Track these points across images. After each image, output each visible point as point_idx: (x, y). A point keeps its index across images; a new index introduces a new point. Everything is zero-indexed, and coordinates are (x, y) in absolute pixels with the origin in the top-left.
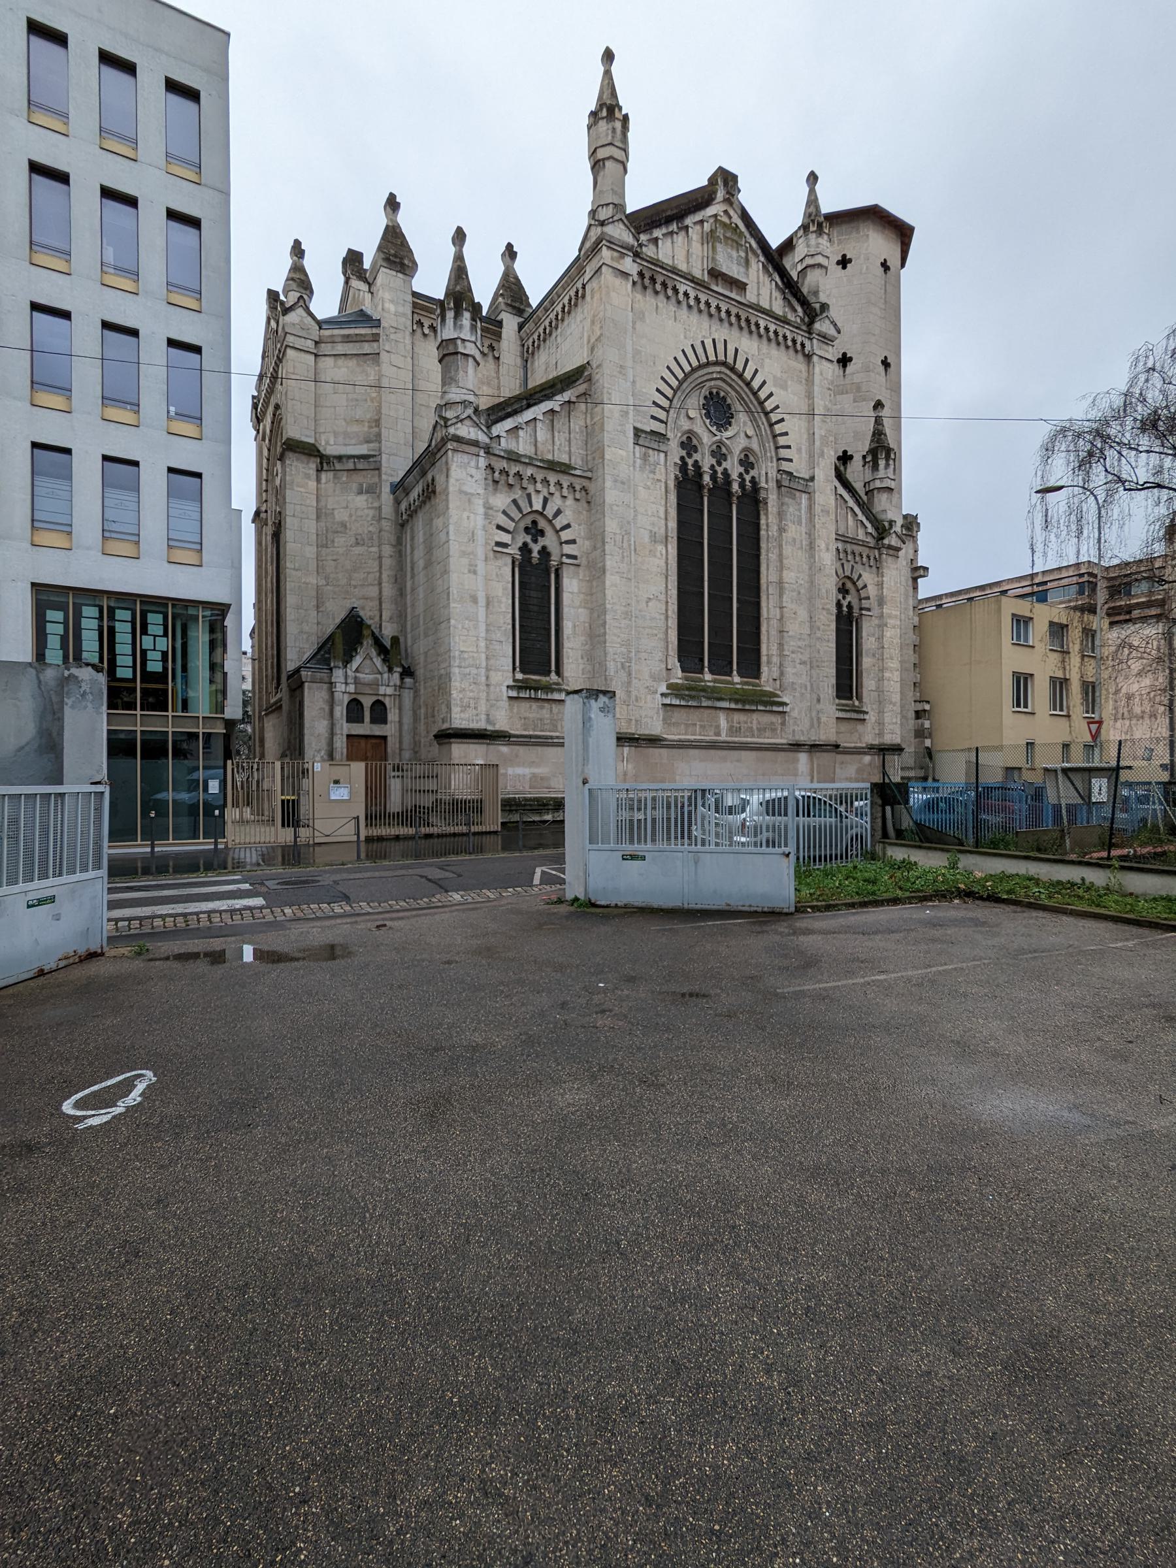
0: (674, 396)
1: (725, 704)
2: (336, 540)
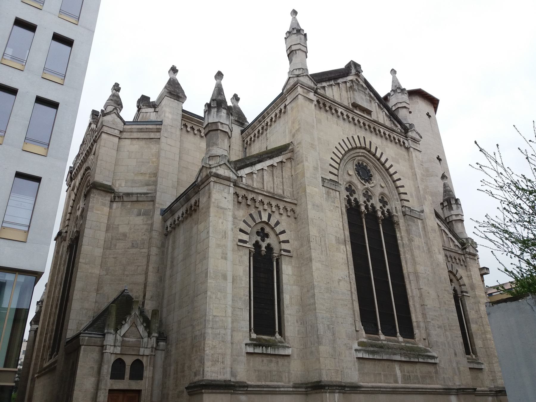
0: (340, 162)
1: (398, 358)
2: (118, 244)
